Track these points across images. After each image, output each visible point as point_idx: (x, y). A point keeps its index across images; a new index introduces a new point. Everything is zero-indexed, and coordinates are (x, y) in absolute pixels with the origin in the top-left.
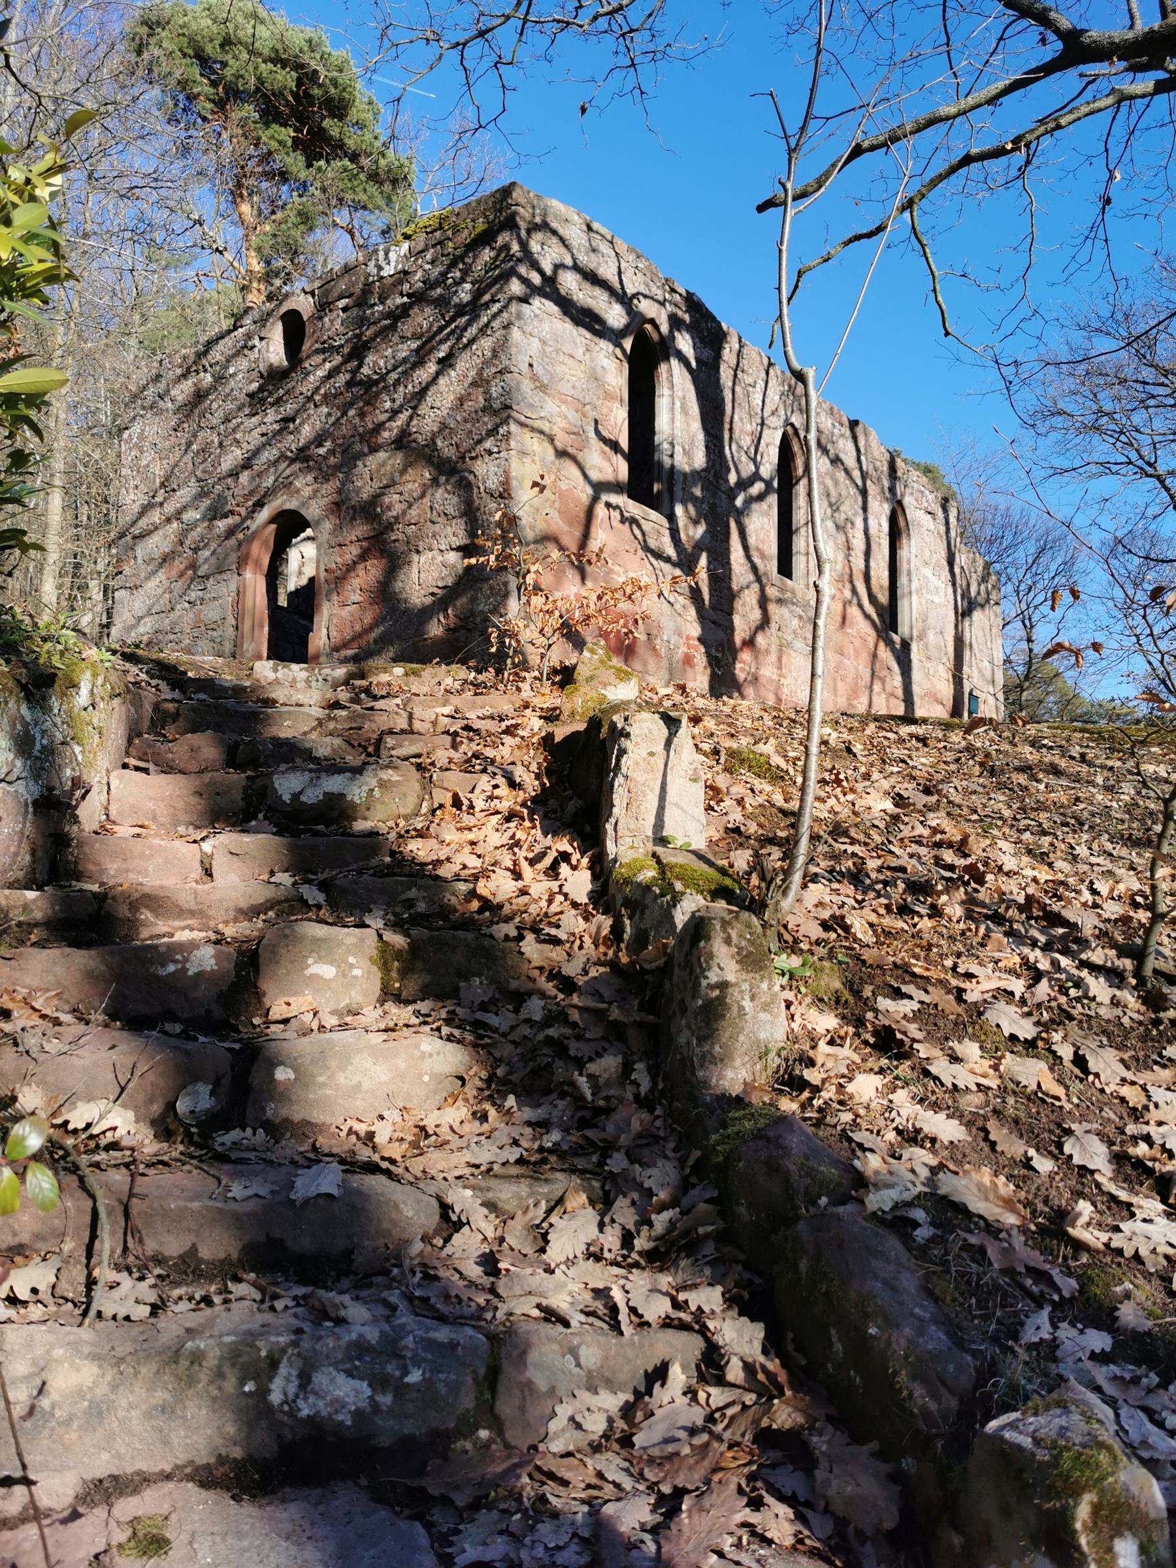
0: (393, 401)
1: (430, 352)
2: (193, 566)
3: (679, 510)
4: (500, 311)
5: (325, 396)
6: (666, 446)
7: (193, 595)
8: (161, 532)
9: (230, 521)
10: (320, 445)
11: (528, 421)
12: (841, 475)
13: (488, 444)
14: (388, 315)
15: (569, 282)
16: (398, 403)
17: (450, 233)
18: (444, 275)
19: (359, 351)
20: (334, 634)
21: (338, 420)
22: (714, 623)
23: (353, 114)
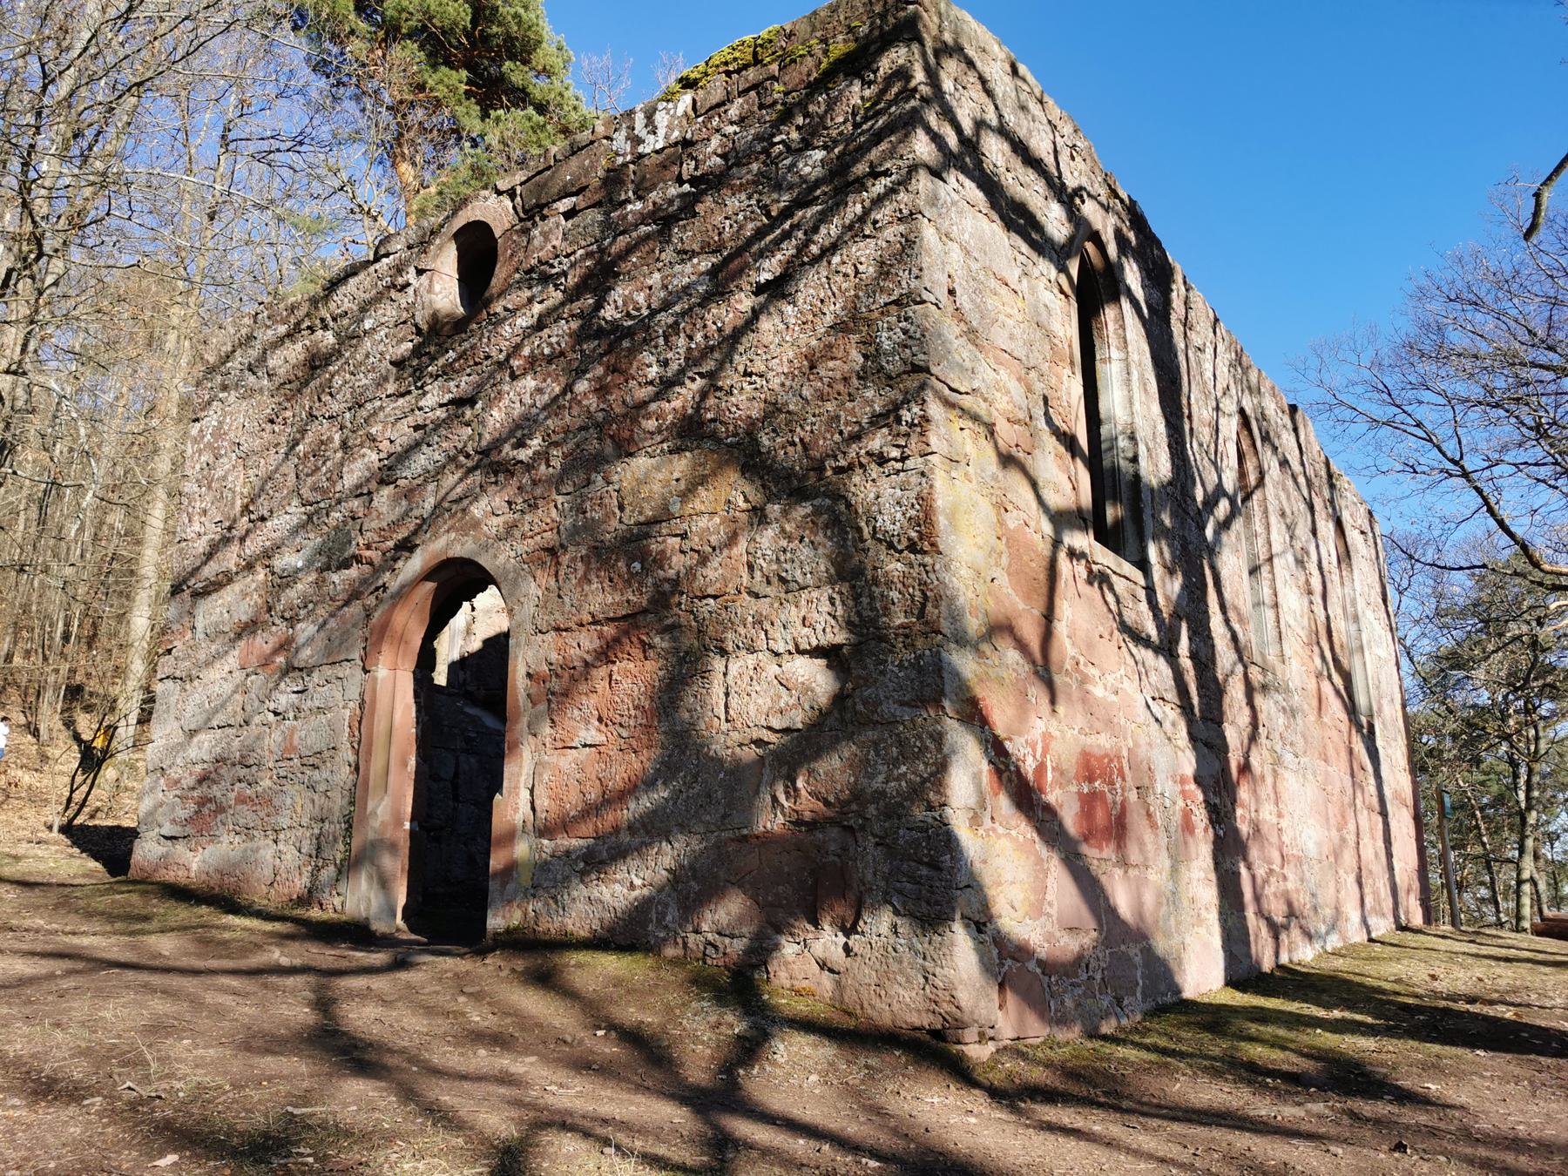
0: (665, 364)
1: (740, 272)
2: (285, 645)
3: (1152, 552)
4: (892, 191)
5: (532, 362)
6: (1123, 443)
7: (284, 699)
8: (236, 587)
9: (353, 572)
10: (520, 444)
11: (954, 397)
12: (1290, 483)
13: (876, 442)
14: (654, 216)
15: (995, 151)
16: (674, 367)
17: (774, 67)
18: (766, 139)
19: (601, 277)
20: (543, 802)
21: (555, 399)
22: (1206, 744)
23: (540, 58)
